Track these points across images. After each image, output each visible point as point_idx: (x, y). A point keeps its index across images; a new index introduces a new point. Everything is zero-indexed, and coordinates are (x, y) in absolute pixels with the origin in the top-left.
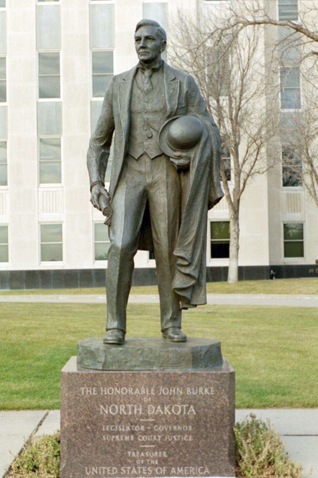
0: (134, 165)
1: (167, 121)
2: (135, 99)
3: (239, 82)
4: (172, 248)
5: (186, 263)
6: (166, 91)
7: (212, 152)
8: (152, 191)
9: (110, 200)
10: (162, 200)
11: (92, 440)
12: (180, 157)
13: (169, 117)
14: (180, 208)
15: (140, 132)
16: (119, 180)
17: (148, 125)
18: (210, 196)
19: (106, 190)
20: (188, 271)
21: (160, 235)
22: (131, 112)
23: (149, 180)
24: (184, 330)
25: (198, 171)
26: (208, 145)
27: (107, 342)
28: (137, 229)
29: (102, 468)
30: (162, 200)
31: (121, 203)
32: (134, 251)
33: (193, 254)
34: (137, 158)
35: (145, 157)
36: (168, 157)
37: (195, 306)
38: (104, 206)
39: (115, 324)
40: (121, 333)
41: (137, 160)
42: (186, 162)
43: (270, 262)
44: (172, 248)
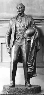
4: (27, 62)
6: (25, 94)
7: (37, 37)
9: (11, 50)
10: (24, 49)
12: (28, 39)
14: (29, 50)
15: (18, 33)
16: (13, 45)
17: (20, 30)
18: (37, 49)
20: (31, 68)
22: (16, 27)
23: (21, 44)
24: (31, 83)
25: (33, 42)
26: (36, 35)
30: (24, 49)
31: (14, 50)
33: (33, 63)
35: (20, 38)
37: (34, 77)
38: (9, 52)
39: (12, 82)
41: (18, 39)
43: (42, 74)
44: (27, 62)
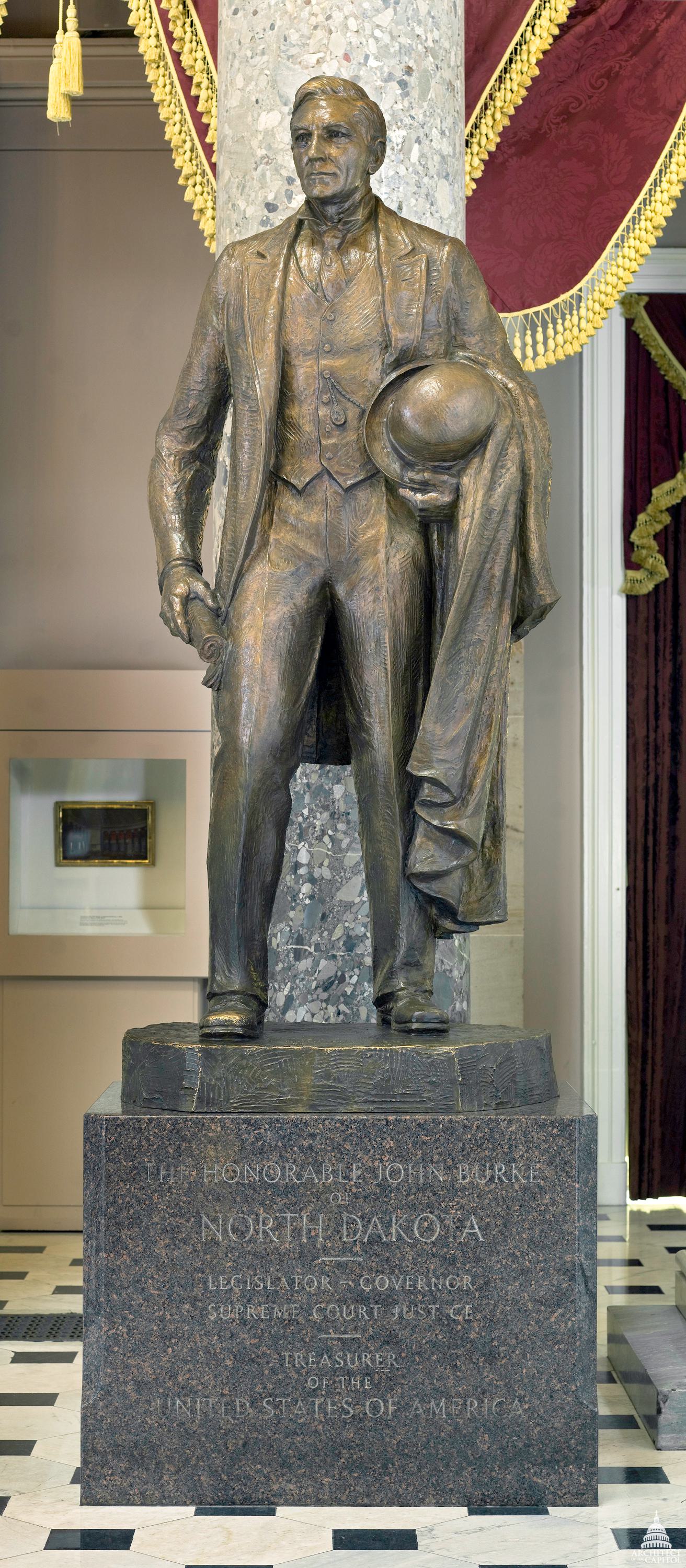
0: (289, 503)
1: (394, 375)
2: (289, 326)
3: (471, 511)
5: (446, 797)
8: (341, 590)
11: (254, 1292)
12: (424, 487)
13: (397, 364)
17: (333, 387)
19: (207, 585)
21: (370, 716)
27: (207, 1031)
28: (299, 697)
29: (79, 1360)
32: (292, 764)
34: (300, 486)
36: (391, 488)
40: (254, 1004)
42: (447, 498)
